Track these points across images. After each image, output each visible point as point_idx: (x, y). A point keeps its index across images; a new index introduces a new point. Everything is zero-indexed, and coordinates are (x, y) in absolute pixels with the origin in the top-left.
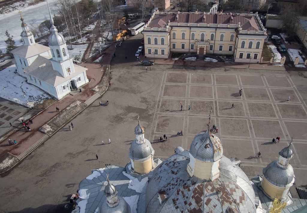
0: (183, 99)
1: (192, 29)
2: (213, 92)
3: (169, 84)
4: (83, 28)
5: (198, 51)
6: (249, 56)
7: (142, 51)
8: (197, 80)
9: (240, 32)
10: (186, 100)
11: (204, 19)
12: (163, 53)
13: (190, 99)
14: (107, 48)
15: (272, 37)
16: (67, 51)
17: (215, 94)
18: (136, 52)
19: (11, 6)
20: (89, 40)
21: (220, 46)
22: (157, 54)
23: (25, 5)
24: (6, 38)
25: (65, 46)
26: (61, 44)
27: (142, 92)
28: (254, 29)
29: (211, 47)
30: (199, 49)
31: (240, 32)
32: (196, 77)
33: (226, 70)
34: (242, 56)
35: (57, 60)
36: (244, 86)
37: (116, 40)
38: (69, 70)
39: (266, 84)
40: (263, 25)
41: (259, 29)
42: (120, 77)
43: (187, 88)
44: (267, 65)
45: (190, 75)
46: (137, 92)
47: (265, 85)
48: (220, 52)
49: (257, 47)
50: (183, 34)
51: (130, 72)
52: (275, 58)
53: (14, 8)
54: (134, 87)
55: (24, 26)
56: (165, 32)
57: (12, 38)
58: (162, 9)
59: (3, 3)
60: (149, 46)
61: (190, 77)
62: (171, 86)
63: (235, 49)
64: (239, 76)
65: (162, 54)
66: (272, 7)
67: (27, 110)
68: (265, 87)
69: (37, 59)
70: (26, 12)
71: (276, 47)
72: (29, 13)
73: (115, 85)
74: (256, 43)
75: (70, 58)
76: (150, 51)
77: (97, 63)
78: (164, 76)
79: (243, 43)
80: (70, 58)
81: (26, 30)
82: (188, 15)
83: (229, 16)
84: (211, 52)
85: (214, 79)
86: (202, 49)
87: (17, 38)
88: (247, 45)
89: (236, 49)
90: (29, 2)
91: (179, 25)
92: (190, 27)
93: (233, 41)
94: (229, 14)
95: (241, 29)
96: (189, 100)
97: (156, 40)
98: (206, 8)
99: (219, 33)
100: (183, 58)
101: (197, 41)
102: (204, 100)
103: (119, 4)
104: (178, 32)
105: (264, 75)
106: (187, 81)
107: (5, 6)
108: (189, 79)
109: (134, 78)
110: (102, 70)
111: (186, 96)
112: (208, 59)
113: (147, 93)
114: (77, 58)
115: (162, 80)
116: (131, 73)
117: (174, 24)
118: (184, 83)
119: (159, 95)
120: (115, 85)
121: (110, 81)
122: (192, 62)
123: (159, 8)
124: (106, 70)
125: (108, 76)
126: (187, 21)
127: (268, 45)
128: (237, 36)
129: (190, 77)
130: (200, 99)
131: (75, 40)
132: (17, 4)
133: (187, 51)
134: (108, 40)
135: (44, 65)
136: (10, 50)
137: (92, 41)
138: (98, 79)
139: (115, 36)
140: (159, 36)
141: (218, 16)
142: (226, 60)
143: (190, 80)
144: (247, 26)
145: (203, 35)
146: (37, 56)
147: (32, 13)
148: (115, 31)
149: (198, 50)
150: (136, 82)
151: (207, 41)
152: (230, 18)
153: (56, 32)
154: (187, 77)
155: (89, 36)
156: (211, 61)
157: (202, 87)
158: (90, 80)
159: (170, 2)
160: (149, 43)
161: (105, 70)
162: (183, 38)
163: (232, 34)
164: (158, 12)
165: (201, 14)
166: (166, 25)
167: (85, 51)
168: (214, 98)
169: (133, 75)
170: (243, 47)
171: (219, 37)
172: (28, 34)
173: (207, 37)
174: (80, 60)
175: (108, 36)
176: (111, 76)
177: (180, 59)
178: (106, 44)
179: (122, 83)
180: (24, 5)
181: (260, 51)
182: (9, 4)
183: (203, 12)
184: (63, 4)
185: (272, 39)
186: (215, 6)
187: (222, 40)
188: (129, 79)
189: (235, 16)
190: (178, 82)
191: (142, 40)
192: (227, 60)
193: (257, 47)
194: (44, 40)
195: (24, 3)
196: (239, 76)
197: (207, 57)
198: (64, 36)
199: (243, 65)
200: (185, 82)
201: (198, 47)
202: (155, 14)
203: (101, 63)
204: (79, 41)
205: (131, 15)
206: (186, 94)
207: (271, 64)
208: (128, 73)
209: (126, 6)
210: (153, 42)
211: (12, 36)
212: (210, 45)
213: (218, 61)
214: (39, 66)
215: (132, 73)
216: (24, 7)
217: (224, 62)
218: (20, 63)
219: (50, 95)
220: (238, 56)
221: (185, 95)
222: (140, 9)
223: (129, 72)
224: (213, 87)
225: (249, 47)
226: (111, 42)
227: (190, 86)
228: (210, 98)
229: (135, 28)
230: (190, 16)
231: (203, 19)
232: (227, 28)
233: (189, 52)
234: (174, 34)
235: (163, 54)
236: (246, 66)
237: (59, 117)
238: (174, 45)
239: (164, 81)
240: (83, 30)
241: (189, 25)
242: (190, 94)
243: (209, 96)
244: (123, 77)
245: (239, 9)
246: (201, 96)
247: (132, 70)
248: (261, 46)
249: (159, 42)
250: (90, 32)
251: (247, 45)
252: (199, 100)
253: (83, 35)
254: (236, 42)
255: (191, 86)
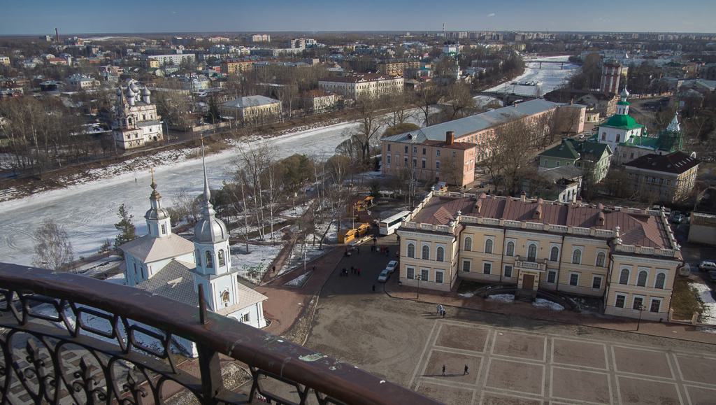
0: (471, 389)
1: (510, 233)
2: (543, 380)
3: (442, 349)
4: (280, 211)
5: (520, 282)
6: (638, 303)
7: (395, 270)
8: (510, 347)
9: (618, 248)
10: (475, 391)
11: (538, 213)
12: (439, 280)
13: (485, 389)
14: (322, 257)
15: (702, 266)
16: (227, 256)
17: (547, 385)
18: (382, 270)
19: (152, 157)
20: (286, 237)
21: (572, 275)
22: (427, 280)
23: (180, 157)
24: (119, 220)
25: (225, 245)
26: (217, 240)
27: (378, 362)
28: (651, 243)
29: (552, 275)
30: (522, 278)
31: (618, 248)
32: (509, 341)
33: (580, 333)
34: (623, 301)
35: (204, 273)
36: (620, 372)
37: (343, 243)
38: (226, 295)
39: (677, 374)
40: (674, 235)
41: (664, 245)
42: (336, 322)
43: (482, 364)
44: (683, 328)
45: (494, 334)
46: (366, 360)
47: (673, 375)
48: (573, 289)
49: (659, 285)
50: (489, 243)
51: (360, 315)
52: (704, 314)
53: (157, 162)
54: (361, 349)
55: (156, 199)
56: (447, 234)
57: (130, 220)
58: (455, 185)
59: (139, 151)
60: (410, 260)
61: (494, 340)
62: (446, 354)
63: (608, 284)
64: (612, 348)
65: (437, 281)
66: (707, 198)
67: (124, 371)
68: (674, 381)
69: (169, 266)
70: (179, 170)
71: (709, 289)
72: (185, 174)
73: (321, 338)
74: (619, 272)
75: (233, 271)
76: (410, 271)
77: (292, 288)
78: (435, 330)
79: (625, 274)
80: (233, 271)
81: (158, 207)
82: (503, 203)
83: (595, 212)
84: (552, 286)
85: (549, 349)
86: (529, 279)
87: (139, 220)
88: (633, 278)
89: (609, 285)
90: (188, 152)
91: (481, 221)
92: (505, 228)
93: (602, 266)
94: (597, 207)
95: (620, 241)
96: (483, 391)
97: (426, 249)
98: (551, 190)
99: (570, 245)
100: (482, 295)
101: (521, 259)
102: (519, 397)
103: (365, 169)
104: (478, 236)
105: (674, 352)
106: (486, 346)
107: (141, 156)
108: (490, 343)
109: (366, 328)
110: (300, 304)
111: (477, 382)
112: (541, 302)
113: (389, 366)
114: (253, 273)
115: (429, 340)
116: (361, 317)
117: (471, 218)
118: (478, 351)
119: (415, 373)
120: (321, 338)
121: (312, 329)
122: (502, 305)
123: (450, 183)
124: (308, 304)
125: (309, 318)
126: (500, 215)
127: (692, 281)
128: (611, 258)
129: (494, 340)
130: (509, 393)
131: (259, 236)
132: (166, 154)
133: (497, 279)
134: (326, 241)
135: (179, 280)
136: (122, 243)
137: (292, 240)
138: (288, 323)
139: (341, 235)
140: (434, 242)
141: (570, 211)
142: (583, 306)
143: (493, 345)
144: (637, 236)
145: (532, 248)
146: (170, 260)
147: (190, 173)
148: (344, 222)
149: (521, 280)
150: (369, 338)
151: (541, 262)
152: (598, 214)
153: (212, 215)
154: (487, 339)
155: (288, 229)
156: (548, 307)
157: (519, 365)
158: (268, 323)
159: (475, 173)
160: (411, 255)
161: (306, 303)
162: (488, 251)
163: (601, 250)
164: (443, 191)
165: (533, 202)
166: (451, 220)
167: (274, 260)
168: (542, 395)
169: (365, 322)
170: (624, 281)
171: (577, 257)
172: (161, 214)
173: (544, 252)
174: (259, 277)
175: (326, 232)
176: (317, 319)
177: (479, 295)
178: (320, 250)
179: (337, 335)
180: (177, 157)
181: (666, 293)
182: (150, 152)
183: (538, 198)
184: (248, 161)
185: (701, 270)
186: (573, 188)
187: (576, 262)
188: (355, 330)
189: (610, 212)
190: (464, 348)
191: (397, 247)
192: (587, 309)
193: (659, 285)
194: (189, 225)
195: (179, 153)
196: (612, 348)
197: (539, 296)
198: (230, 227)
199: (625, 324)
200: (481, 349)
201: (520, 272)
202: (433, 196)
203: (300, 289)
204: (267, 238)
205: (387, 192)
206: (478, 378)
207: (693, 328)
208: (356, 316)
209: (380, 173)
210: (418, 252)
211: (131, 216)
212: (548, 270)
213: (565, 309)
214: (169, 280)
215: (364, 316)
216: (177, 161)
217: (579, 312)
218: (134, 272)
219: (177, 344)
220: (612, 300)
221: (475, 379)
222: (407, 182)
223: (357, 315)
224: (544, 368)
225: (639, 282)
226: (334, 249)
227: (490, 360)
228: (534, 392)
229: (388, 221)
230: (507, 205)
231: (474, 209)
232: (521, 229)
233: (500, 282)
234: (468, 241)
235: (411, 278)
236: (631, 327)
237: (185, 397)
238: (467, 264)
239: (431, 341)
240: (279, 216)
241: (503, 222)
242: (488, 377)
243: (533, 387)
244: (343, 322)
245: (629, 197)
246: (512, 386)
247: (365, 310)
248: (669, 282)
249: (433, 254)
250: (292, 222)
251: (633, 278)
252: (506, 394)
253: (279, 226)
254: (609, 268)
255: (493, 361)
